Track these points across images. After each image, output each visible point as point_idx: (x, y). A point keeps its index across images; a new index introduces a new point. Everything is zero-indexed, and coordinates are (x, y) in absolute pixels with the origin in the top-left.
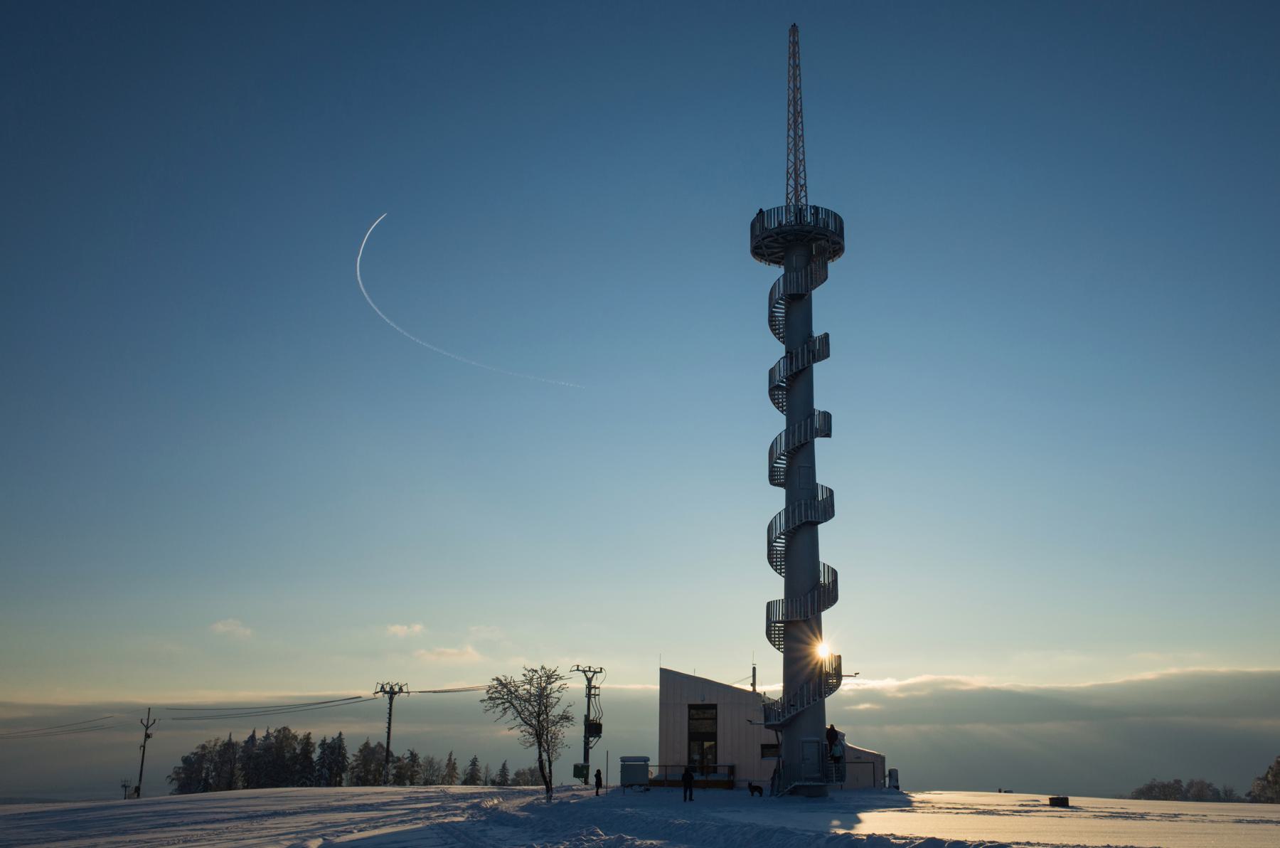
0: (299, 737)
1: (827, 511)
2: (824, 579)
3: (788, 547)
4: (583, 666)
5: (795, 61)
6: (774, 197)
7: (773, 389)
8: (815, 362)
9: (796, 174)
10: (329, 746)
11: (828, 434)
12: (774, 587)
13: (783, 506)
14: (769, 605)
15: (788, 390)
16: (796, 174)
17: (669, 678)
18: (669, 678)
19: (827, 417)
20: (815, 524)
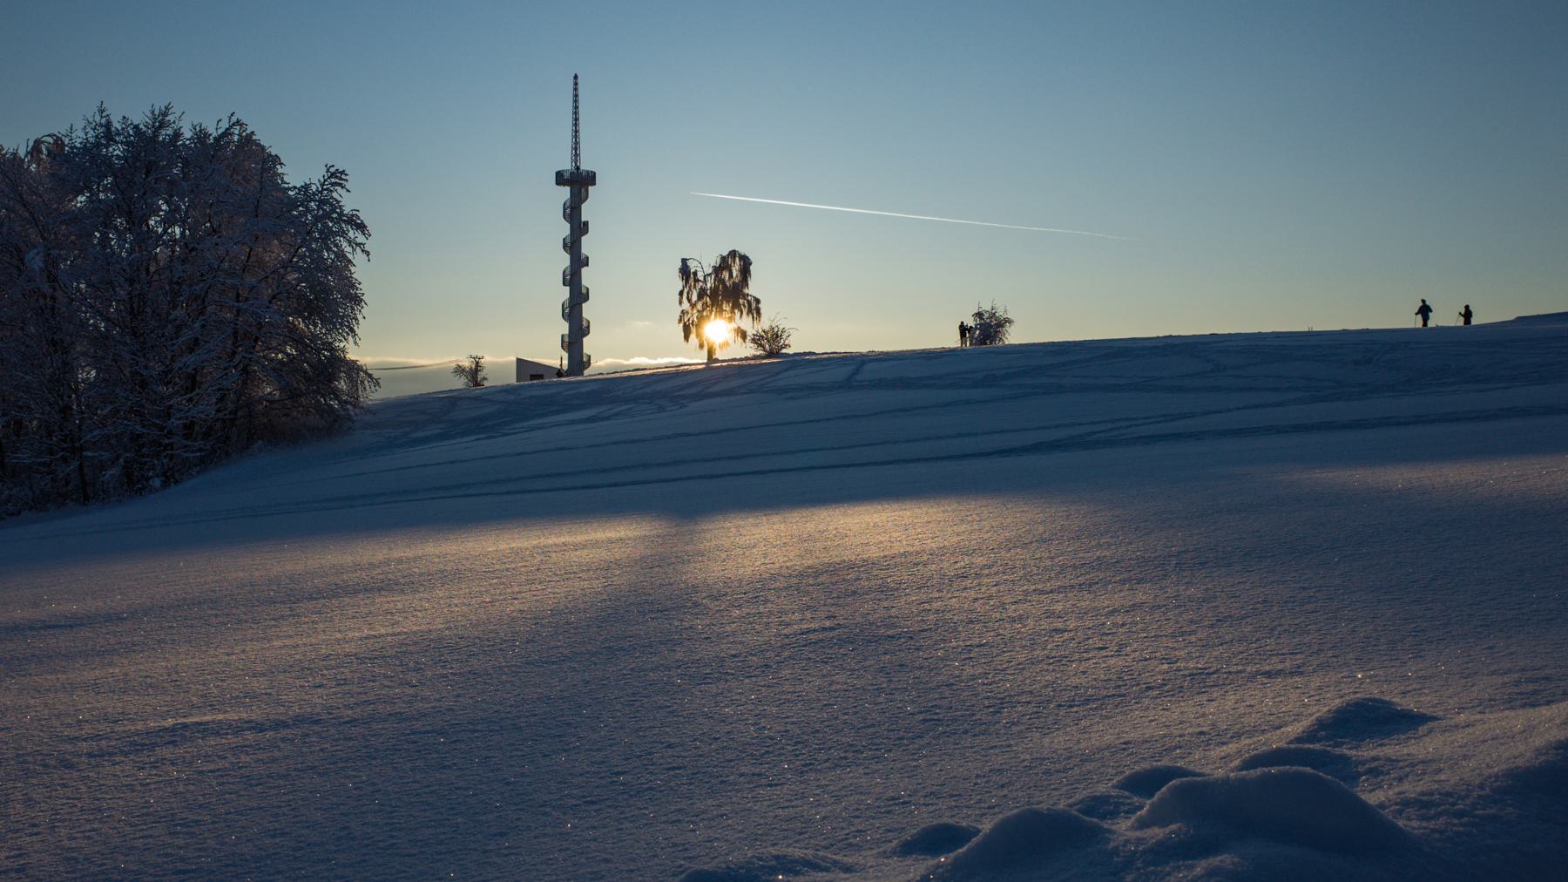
0: (56, 293)
1: (586, 298)
2: (584, 291)
3: (571, 279)
4: (474, 355)
5: (576, 152)
6: (567, 165)
7: (565, 246)
8: (583, 235)
9: (576, 155)
10: (67, 159)
11: (587, 265)
12: (564, 328)
13: (569, 232)
14: (562, 336)
15: (571, 248)
16: (576, 155)
17: (518, 360)
18: (518, 360)
19: (586, 224)
20: (581, 304)
